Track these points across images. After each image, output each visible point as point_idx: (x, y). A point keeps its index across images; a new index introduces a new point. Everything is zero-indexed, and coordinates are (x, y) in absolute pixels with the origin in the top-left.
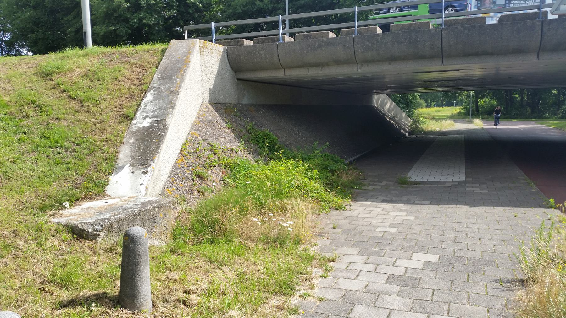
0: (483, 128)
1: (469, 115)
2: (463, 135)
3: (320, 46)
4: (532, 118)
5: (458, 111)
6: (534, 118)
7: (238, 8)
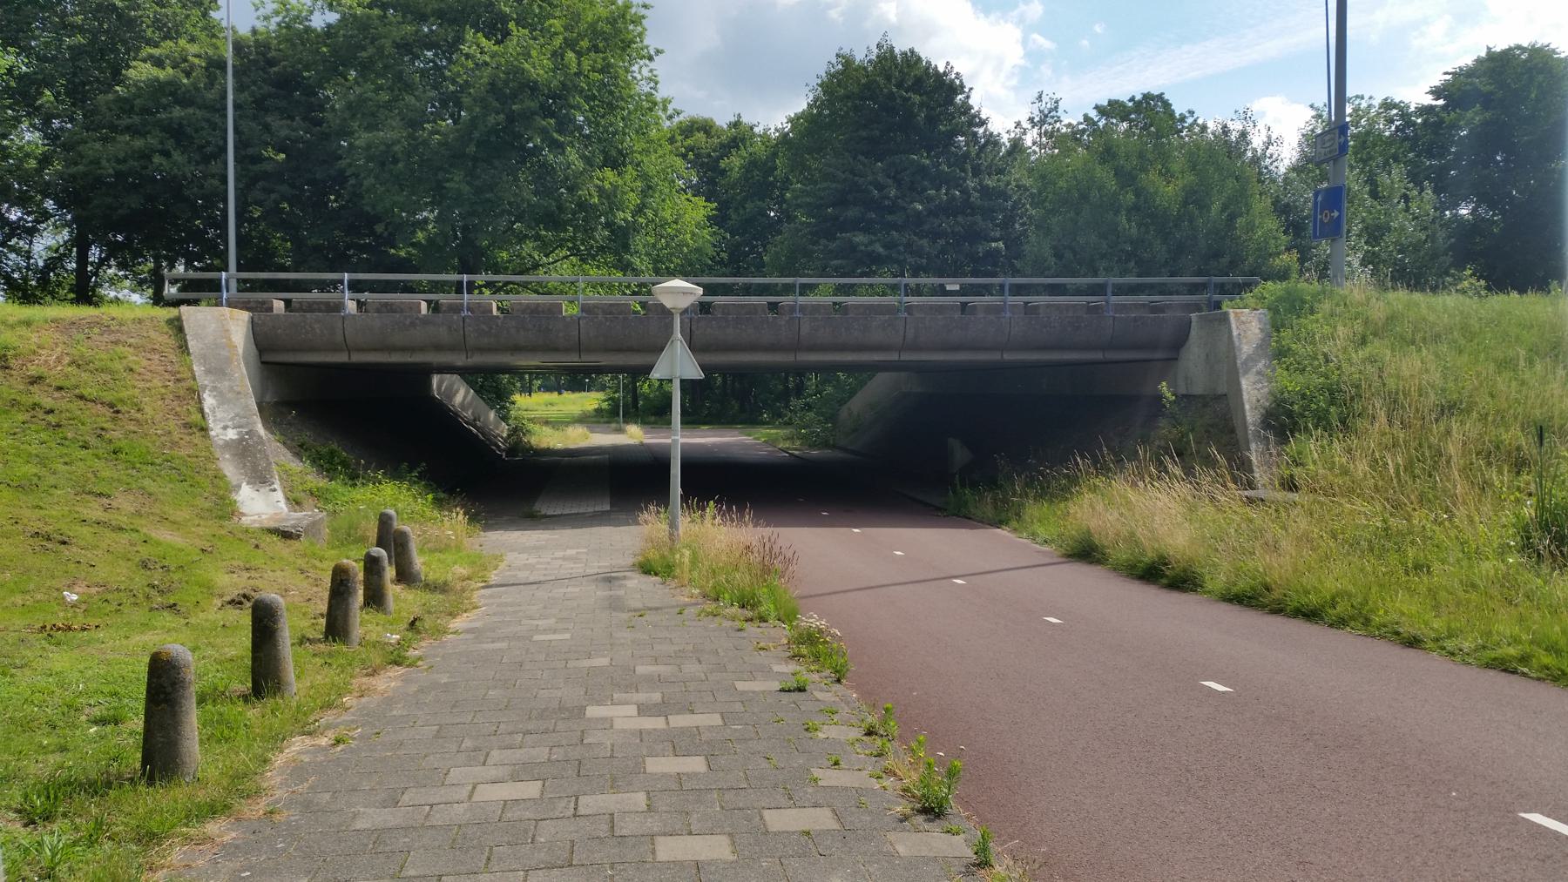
0: (642, 444)
1: (618, 415)
2: (607, 456)
3: (413, 324)
4: (737, 424)
5: (596, 407)
6: (740, 424)
7: (104, 163)
